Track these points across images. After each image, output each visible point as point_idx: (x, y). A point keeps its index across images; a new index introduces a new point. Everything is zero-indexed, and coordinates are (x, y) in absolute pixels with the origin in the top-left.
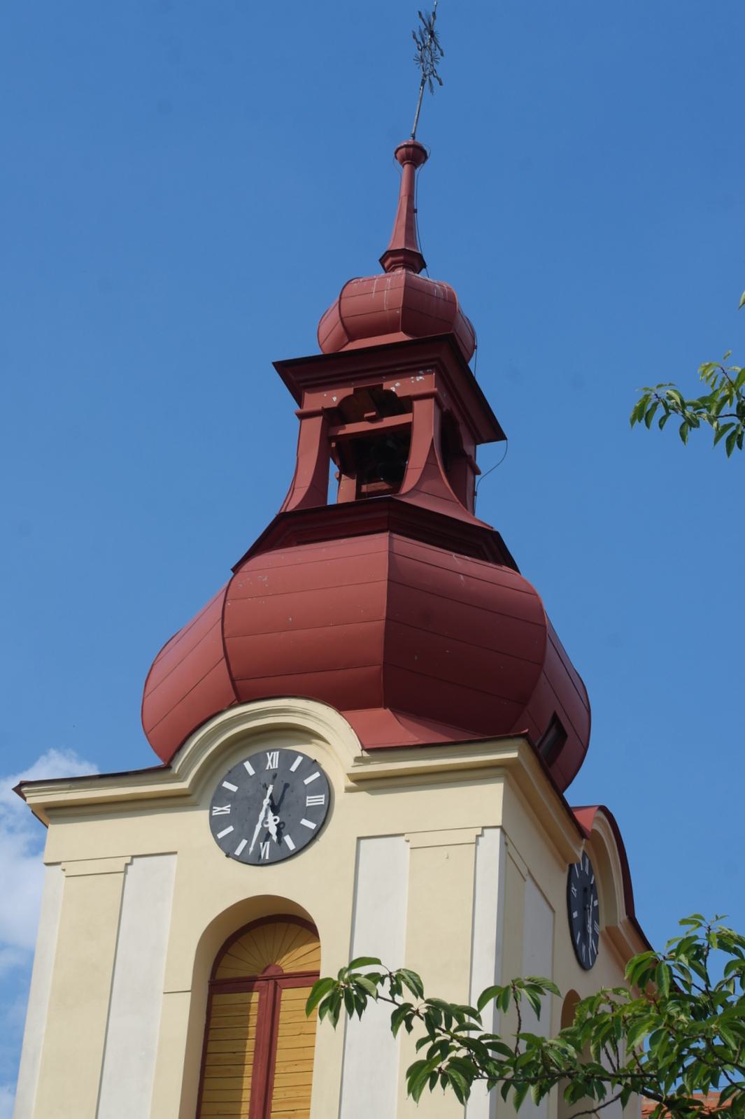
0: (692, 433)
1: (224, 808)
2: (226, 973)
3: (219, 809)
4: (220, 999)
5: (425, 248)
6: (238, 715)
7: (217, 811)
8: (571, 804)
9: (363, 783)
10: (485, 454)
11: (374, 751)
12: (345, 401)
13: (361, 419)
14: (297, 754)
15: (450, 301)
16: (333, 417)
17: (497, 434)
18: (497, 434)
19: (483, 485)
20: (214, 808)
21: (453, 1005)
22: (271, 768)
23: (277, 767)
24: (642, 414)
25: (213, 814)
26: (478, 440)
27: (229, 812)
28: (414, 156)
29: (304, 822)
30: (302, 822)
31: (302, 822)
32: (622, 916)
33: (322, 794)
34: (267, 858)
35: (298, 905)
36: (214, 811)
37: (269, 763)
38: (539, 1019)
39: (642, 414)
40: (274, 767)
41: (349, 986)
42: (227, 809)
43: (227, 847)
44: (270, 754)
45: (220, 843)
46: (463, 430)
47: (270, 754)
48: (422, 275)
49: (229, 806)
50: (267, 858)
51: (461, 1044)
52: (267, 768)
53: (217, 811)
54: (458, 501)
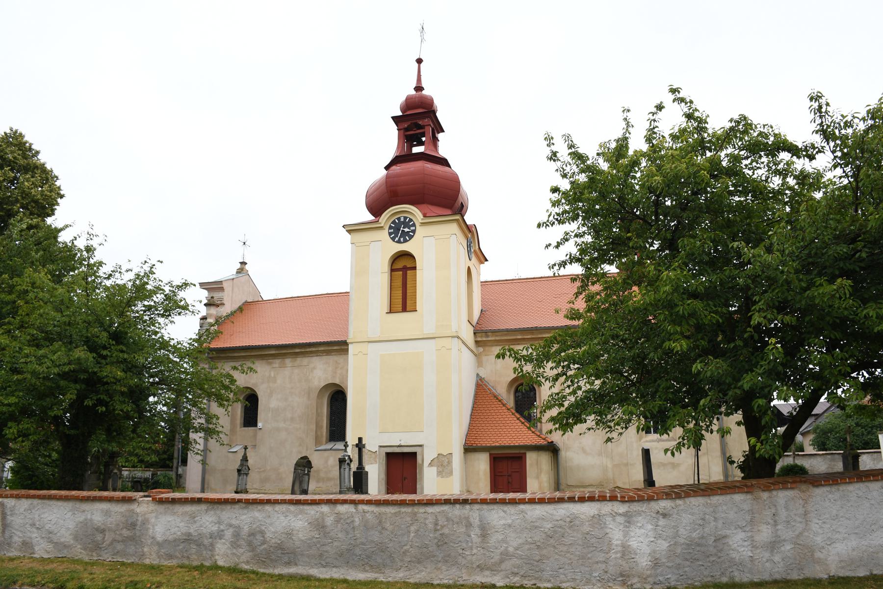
0: (566, 266)
2: (393, 268)
4: (393, 273)
5: (424, 85)
7: (390, 231)
8: (468, 224)
9: (423, 224)
10: (440, 136)
11: (425, 216)
12: (408, 126)
13: (412, 130)
15: (432, 100)
16: (406, 130)
17: (443, 131)
18: (443, 131)
19: (440, 144)
24: (539, 226)
26: (438, 133)
28: (419, 61)
32: (477, 247)
34: (842, 452)
39: (539, 226)
42: (392, 230)
43: (393, 239)
45: (391, 238)
46: (436, 131)
48: (424, 92)
51: (783, 445)
53: (390, 231)
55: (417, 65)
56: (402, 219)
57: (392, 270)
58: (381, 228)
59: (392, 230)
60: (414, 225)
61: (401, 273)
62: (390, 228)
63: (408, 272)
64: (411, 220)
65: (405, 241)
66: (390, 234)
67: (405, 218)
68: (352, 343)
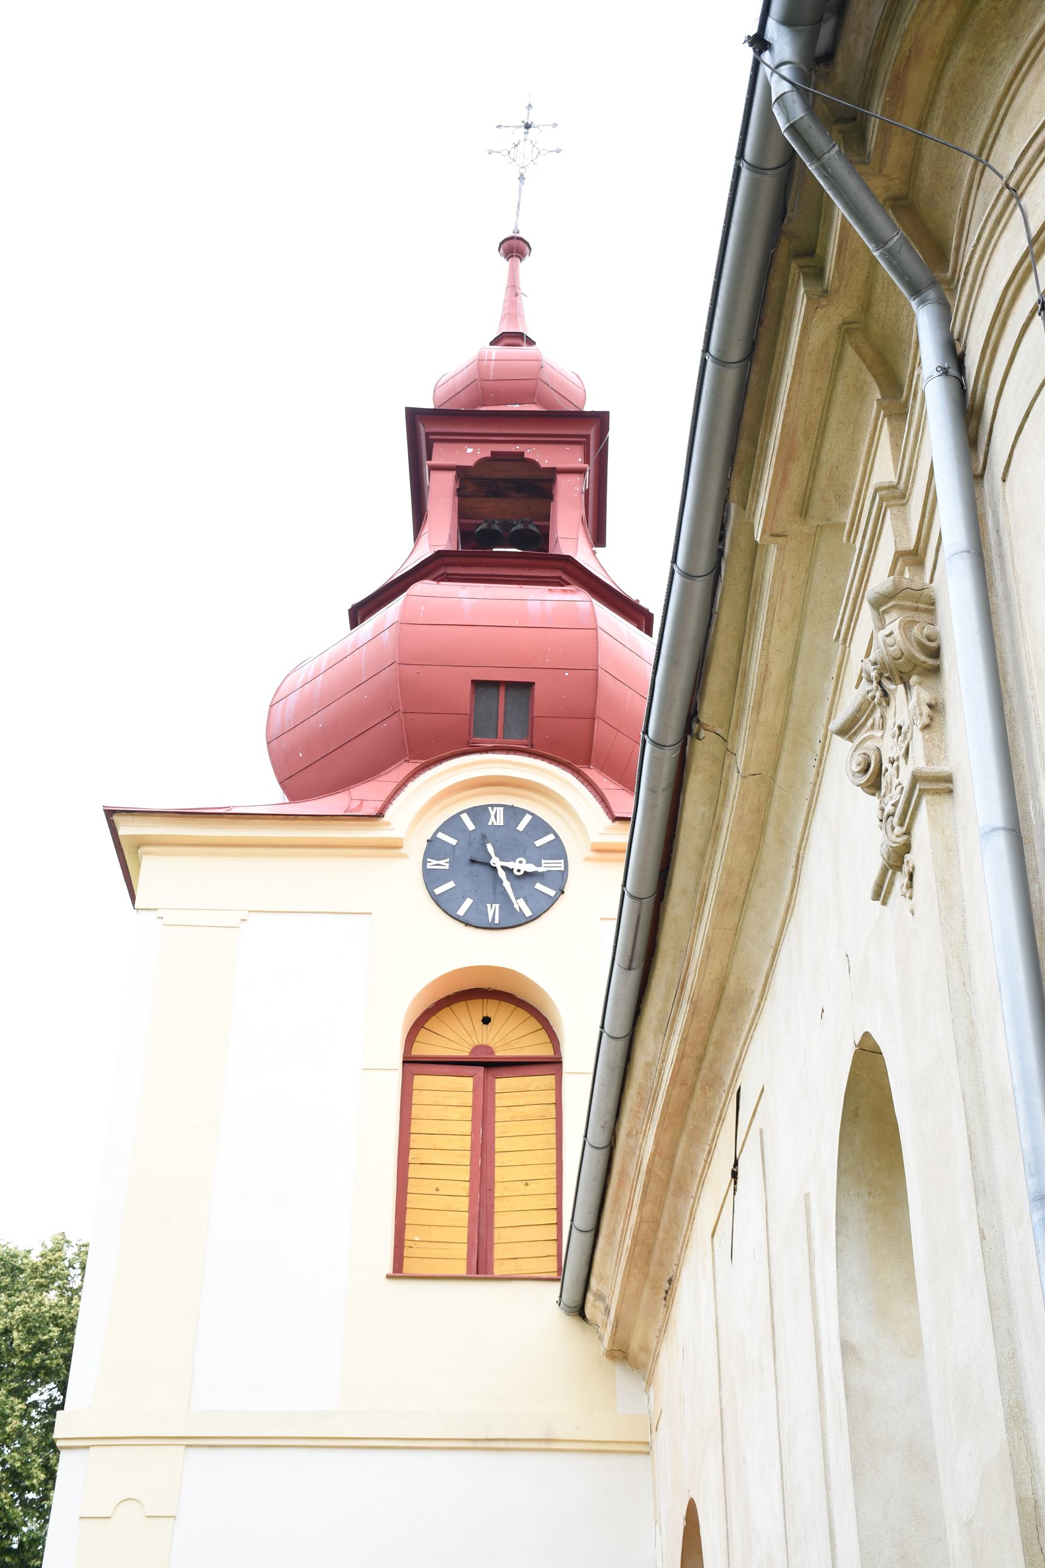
1: (441, 862)
3: (435, 862)
6: (817, 784)
14: (524, 812)
20: (428, 860)
21: (46, 1540)
22: (495, 824)
23: (502, 824)
25: (428, 867)
27: (447, 868)
29: (468, 902)
30: (536, 887)
31: (536, 887)
33: (561, 859)
34: (497, 921)
35: (522, 975)
36: (428, 864)
37: (492, 819)
38: (763, 1086)
40: (498, 824)
41: (31, 1344)
42: (444, 864)
44: (493, 809)
47: (493, 809)
49: (448, 860)
50: (497, 921)
52: (490, 823)
54: (440, 408)
55: (554, 149)
56: (497, 818)
57: (412, 1063)
58: (392, 847)
59: (444, 864)
60: (557, 850)
61: (468, 1083)
62: (433, 847)
63: (503, 1084)
64: (540, 826)
65: (512, 921)
66: (431, 879)
67: (514, 813)
68: (84, 1444)
